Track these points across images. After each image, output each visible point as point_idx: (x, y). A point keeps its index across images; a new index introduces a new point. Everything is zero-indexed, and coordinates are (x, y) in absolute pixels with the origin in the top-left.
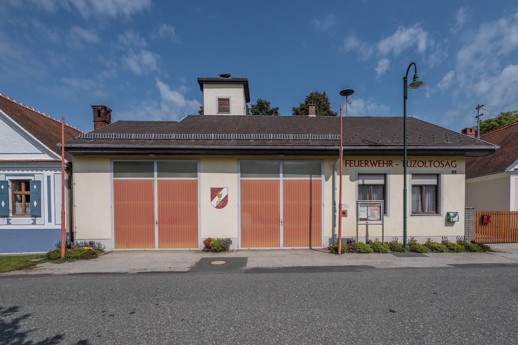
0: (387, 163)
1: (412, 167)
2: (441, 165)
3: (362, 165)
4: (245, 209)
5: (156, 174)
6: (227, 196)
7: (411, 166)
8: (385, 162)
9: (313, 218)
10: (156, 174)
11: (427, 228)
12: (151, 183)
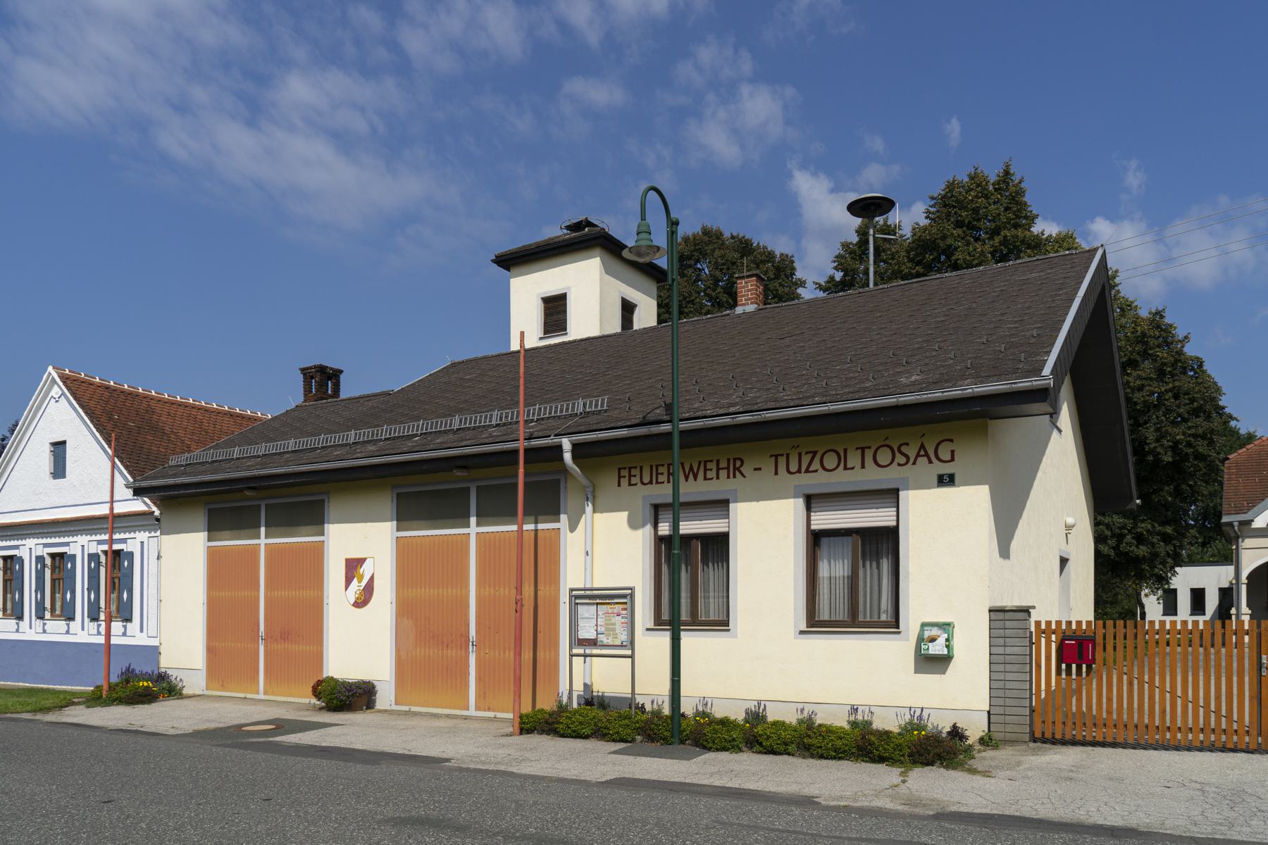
0: (728, 468)
3: (661, 478)
4: (405, 609)
5: (473, 520)
6: (372, 578)
7: (799, 471)
8: (723, 464)
9: (540, 636)
10: (473, 520)
11: (864, 678)
12: (254, 551)
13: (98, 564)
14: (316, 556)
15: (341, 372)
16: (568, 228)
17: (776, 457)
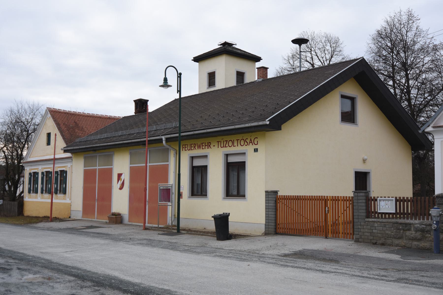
1: (224, 148)
2: (246, 144)
8: (206, 144)
13: (58, 175)
14: (110, 171)
15: (148, 101)
16: (221, 45)
17: (218, 142)
